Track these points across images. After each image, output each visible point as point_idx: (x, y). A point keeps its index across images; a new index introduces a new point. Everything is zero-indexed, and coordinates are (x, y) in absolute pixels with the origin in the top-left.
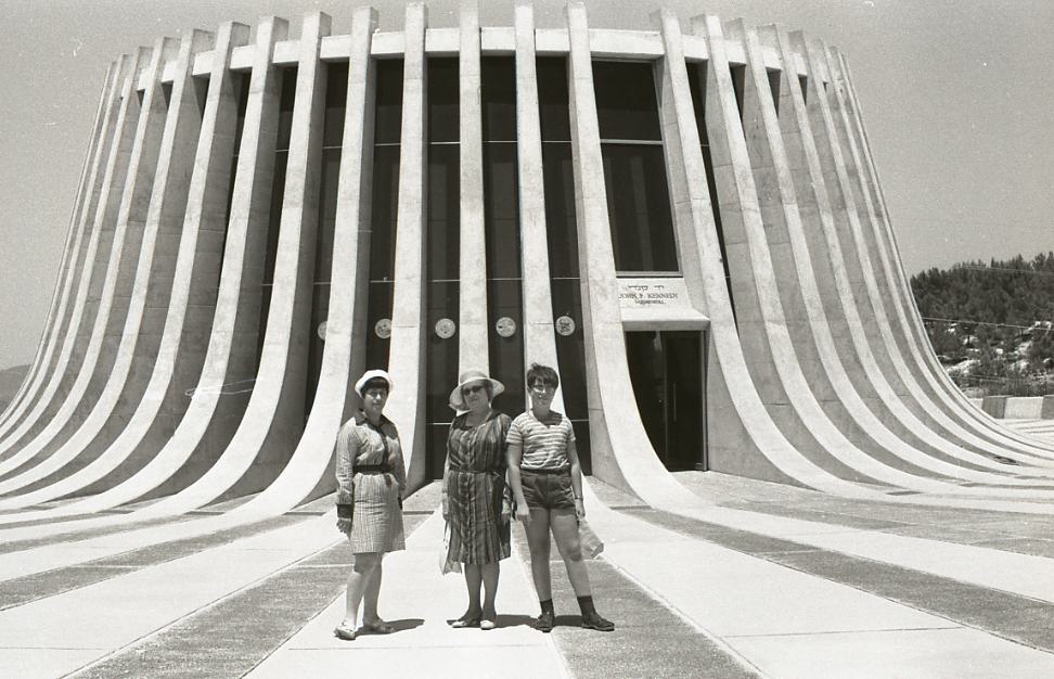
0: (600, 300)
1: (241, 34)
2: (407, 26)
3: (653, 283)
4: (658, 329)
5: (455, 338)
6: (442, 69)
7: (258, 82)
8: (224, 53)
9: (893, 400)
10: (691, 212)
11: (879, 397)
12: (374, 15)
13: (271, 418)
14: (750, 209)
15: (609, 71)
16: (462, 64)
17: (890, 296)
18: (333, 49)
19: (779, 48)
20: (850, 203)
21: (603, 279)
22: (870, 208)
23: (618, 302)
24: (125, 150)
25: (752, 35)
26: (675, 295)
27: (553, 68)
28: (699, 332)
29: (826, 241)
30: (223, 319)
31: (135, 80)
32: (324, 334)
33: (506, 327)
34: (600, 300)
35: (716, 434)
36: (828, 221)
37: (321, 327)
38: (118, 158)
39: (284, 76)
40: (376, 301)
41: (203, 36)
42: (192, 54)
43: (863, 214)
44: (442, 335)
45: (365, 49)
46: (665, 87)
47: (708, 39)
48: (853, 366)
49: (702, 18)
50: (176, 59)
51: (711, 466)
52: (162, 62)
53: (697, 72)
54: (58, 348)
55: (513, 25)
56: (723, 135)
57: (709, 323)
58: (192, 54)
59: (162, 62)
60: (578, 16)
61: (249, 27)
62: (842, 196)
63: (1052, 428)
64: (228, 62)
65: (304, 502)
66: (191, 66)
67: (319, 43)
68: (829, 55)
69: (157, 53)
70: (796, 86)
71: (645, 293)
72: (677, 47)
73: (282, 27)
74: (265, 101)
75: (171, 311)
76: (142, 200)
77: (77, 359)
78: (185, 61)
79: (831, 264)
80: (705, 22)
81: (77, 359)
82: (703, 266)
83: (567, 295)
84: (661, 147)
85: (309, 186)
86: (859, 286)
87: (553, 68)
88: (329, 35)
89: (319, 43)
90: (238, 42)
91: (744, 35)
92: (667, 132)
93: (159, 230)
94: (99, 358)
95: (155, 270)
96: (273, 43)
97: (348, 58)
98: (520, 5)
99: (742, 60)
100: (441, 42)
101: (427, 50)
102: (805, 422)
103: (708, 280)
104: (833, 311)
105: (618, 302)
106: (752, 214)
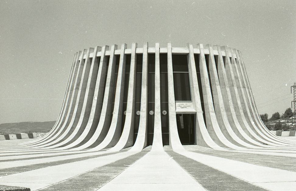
0: (171, 107)
1: (107, 48)
2: (132, 47)
3: (185, 103)
4: (182, 114)
5: (154, 114)
6: (139, 57)
7: (102, 59)
8: (95, 53)
9: (241, 130)
10: (193, 88)
11: (237, 129)
12: (137, 44)
13: (101, 131)
14: (207, 87)
15: (176, 57)
16: (143, 56)
17: (245, 106)
18: (117, 52)
19: (218, 50)
20: (235, 85)
21: (172, 103)
22: (241, 86)
23: (176, 107)
24: (76, 73)
25: (211, 48)
26: (190, 106)
27: (163, 57)
28: (194, 114)
29: (227, 94)
30: (93, 110)
31: (78, 58)
32: (126, 113)
33: (151, 113)
34: (171, 107)
35: (198, 137)
36: (228, 89)
37: (125, 112)
38: (74, 75)
39: (117, 57)
40: (137, 106)
41: (92, 49)
42: (89, 53)
43: (238, 87)
44: (165, 111)
45: (123, 52)
46: (189, 60)
47: (200, 49)
48: (232, 123)
49: (199, 44)
50: (86, 54)
51: (197, 144)
52: (84, 55)
53: (197, 57)
54: (61, 116)
55: (155, 47)
56: (213, 71)
57: (196, 112)
58: (89, 53)
59: (84, 55)
60: (169, 45)
61: (109, 46)
62: (233, 84)
63: (1, 150)
64: (105, 53)
65: (122, 149)
66: (89, 56)
67: (114, 51)
68: (237, 53)
69: (82, 53)
70: (222, 59)
71: (183, 106)
72: (192, 51)
73: (107, 47)
74: (103, 64)
75: (83, 109)
76: (78, 85)
77: (65, 118)
78: (88, 55)
79: (228, 99)
80: (199, 45)
81: (65, 118)
82: (196, 100)
83: (165, 106)
84: (188, 73)
85: (111, 82)
86: (235, 104)
87: (163, 57)
88: (126, 49)
89: (114, 51)
90: (99, 50)
91: (209, 48)
92: (189, 70)
93: (81, 91)
94: (69, 118)
95: (80, 100)
96: (105, 51)
97: (120, 55)
98: (156, 43)
99: (217, 54)
100: (139, 51)
101: (148, 52)
102: (217, 134)
103: (196, 103)
104: (228, 110)
105: (176, 107)
106: (208, 88)
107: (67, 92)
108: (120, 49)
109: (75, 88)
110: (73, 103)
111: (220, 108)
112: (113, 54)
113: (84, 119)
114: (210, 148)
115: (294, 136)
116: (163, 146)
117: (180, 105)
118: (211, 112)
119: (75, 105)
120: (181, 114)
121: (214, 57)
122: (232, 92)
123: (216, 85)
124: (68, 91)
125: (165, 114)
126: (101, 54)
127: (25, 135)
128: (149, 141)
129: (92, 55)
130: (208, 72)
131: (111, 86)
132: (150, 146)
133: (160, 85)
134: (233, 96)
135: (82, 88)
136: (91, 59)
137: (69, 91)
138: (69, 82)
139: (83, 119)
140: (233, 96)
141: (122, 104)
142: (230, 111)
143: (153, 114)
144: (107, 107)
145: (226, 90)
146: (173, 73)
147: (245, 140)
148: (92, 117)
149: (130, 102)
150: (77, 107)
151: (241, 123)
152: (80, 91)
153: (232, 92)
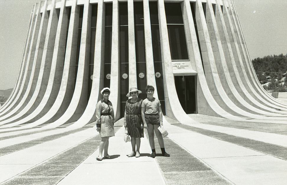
3: (181, 63)
4: (183, 75)
7: (73, 10)
10: (192, 43)
14: (208, 42)
22: (241, 41)
23: (172, 68)
28: (194, 76)
30: (65, 74)
31: (40, 10)
33: (142, 75)
36: (229, 45)
46: (184, 9)
48: (236, 84)
52: (47, 5)
54: (21, 83)
57: (197, 73)
59: (47, 5)
70: (220, 8)
71: (179, 66)
75: (51, 73)
79: (230, 57)
83: (158, 66)
86: (238, 63)
104: (231, 70)
105: (172, 68)
107: (26, 52)
109: (37, 47)
110: (36, 67)
111: (222, 68)
113: (54, 86)
114: (222, 117)
115: (277, 98)
117: (176, 65)
118: (214, 73)
119: (39, 69)
120: (182, 76)
121: (212, 6)
122: (233, 48)
123: (216, 39)
124: (28, 52)
125: (158, 77)
130: (194, 24)
131: (60, 47)
133: (151, 40)
134: (235, 53)
135: (48, 46)
137: (30, 52)
138: (28, 41)
139: (53, 86)
140: (235, 53)
141: (104, 65)
142: (233, 71)
143: (126, 78)
144: (84, 70)
145: (227, 46)
147: (254, 105)
148: (65, 84)
149: (115, 63)
150: (43, 71)
151: (246, 85)
152: (46, 50)
153: (233, 48)
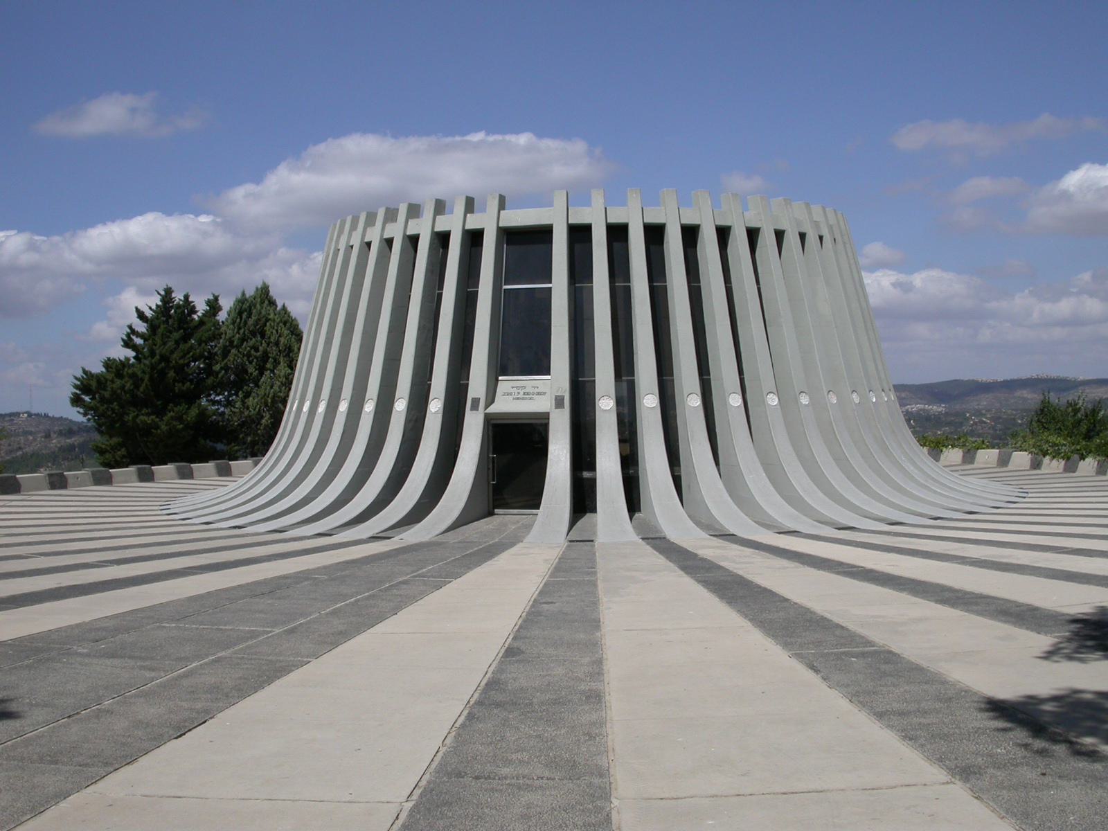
15: (510, 236)
18: (473, 223)
39: (442, 239)
84: (629, 286)
97: (552, 225)
108: (484, 210)
112: (642, 224)
116: (631, 519)
126: (454, 223)
127: (965, 615)
128: (583, 499)
129: (396, 232)
130: (731, 288)
132: (588, 517)
136: (389, 242)
146: (700, 283)
